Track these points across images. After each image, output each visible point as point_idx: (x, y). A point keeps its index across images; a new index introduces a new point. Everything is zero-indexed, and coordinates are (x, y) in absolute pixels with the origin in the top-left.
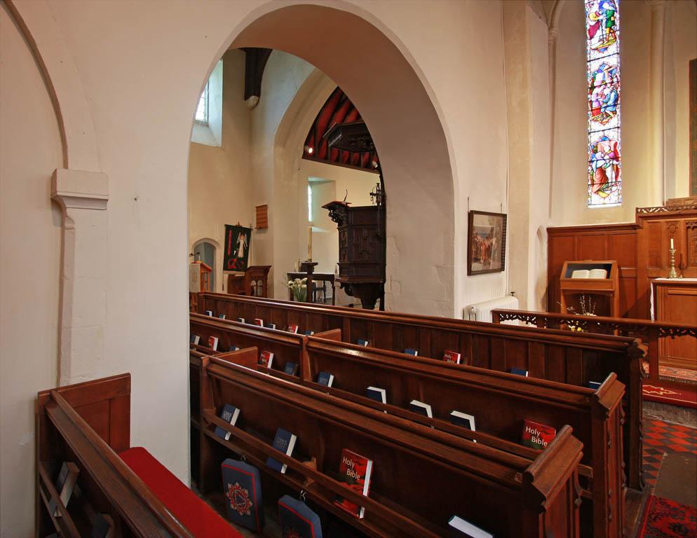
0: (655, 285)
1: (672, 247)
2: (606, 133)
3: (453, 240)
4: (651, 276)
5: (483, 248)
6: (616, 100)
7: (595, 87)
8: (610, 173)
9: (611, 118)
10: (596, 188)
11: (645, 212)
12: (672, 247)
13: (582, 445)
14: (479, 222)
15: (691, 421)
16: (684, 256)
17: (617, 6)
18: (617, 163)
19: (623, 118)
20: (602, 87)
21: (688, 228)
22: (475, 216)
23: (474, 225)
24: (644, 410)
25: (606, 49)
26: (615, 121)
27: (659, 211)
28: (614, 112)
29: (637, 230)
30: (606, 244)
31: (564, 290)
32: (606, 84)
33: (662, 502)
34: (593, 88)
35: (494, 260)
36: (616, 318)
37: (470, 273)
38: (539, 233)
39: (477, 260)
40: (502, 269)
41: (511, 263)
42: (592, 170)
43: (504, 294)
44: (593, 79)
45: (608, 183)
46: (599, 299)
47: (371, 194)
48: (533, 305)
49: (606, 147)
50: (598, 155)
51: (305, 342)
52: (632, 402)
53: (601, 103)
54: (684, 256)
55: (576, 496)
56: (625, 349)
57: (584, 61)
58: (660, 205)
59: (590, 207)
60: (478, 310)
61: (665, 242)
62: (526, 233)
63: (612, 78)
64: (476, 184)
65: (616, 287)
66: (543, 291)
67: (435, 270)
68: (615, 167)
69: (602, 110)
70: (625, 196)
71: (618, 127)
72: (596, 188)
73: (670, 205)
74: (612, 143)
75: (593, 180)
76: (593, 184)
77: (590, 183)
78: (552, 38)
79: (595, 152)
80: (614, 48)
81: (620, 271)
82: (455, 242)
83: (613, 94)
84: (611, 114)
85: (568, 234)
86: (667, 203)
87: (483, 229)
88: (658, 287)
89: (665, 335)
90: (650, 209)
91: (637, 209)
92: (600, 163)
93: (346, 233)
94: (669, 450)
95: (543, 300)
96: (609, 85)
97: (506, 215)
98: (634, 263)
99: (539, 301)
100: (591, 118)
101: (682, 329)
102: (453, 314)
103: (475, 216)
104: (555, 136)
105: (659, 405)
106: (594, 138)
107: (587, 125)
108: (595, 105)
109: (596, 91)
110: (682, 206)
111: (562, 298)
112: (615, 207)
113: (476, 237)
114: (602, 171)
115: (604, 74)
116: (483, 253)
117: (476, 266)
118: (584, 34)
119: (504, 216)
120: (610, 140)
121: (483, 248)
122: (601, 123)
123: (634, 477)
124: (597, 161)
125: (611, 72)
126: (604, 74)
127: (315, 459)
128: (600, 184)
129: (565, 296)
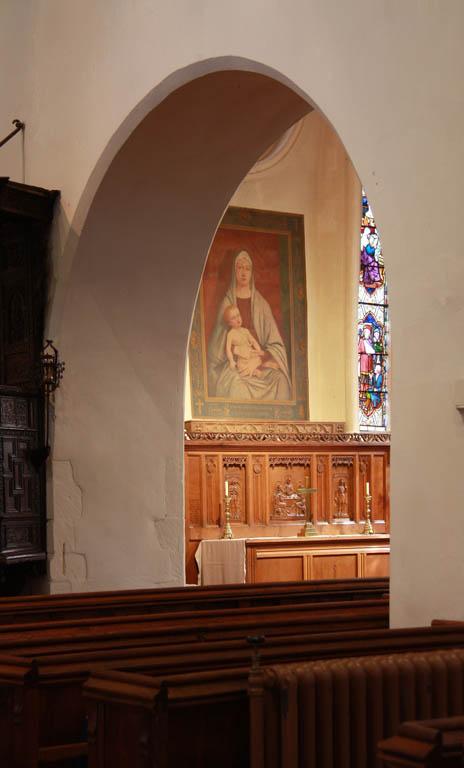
67: (151, 524)
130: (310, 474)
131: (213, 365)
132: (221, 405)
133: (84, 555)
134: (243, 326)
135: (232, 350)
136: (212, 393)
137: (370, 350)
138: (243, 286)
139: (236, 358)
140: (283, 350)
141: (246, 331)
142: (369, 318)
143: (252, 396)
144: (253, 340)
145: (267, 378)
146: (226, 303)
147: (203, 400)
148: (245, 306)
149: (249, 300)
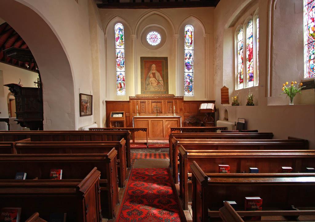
0: (134, 118)
2: (122, 73)
3: (74, 103)
5: (85, 107)
6: (124, 63)
8: (122, 85)
10: (119, 89)
13: (117, 151)
14: (84, 97)
17: (123, 34)
19: (125, 69)
22: (82, 95)
23: (82, 98)
24: (131, 151)
25: (121, 46)
26: (123, 69)
28: (123, 67)
33: (135, 169)
34: (117, 57)
35: (88, 111)
36: (125, 128)
37: (81, 116)
38: (103, 102)
39: (83, 111)
40: (92, 115)
41: (94, 111)
43: (95, 121)
44: (118, 54)
46: (120, 123)
47: (34, 82)
48: (102, 126)
49: (121, 76)
50: (119, 79)
51: (14, 145)
52: (127, 144)
55: (116, 162)
56: (126, 133)
57: (115, 49)
59: (118, 95)
62: (99, 102)
64: (82, 84)
66: (105, 122)
67: (67, 115)
69: (120, 65)
70: (126, 92)
75: (118, 87)
76: (118, 88)
78: (105, 38)
79: (119, 78)
80: (123, 47)
81: (126, 115)
82: (75, 104)
83: (123, 61)
87: (85, 100)
89: (136, 131)
92: (120, 82)
93: (21, 99)
94: (136, 159)
95: (105, 124)
96: (122, 58)
98: (129, 113)
99: (104, 125)
101: (139, 129)
102: (75, 129)
103: (82, 95)
104: (107, 73)
105: (135, 149)
106: (118, 73)
107: (116, 69)
108: (118, 63)
109: (118, 58)
111: (111, 123)
113: (235, 99)
114: (121, 84)
116: (85, 109)
117: (83, 114)
118: (114, 39)
119: (92, 96)
121: (85, 107)
123: (128, 165)
125: (122, 54)
127: (37, 178)
129: (111, 123)
130: (162, 104)
131: (146, 85)
132: (148, 92)
133: (51, 120)
134: (153, 77)
135: (151, 82)
136: (146, 89)
137: (189, 81)
138: (153, 70)
139: (151, 83)
140: (163, 82)
141: (154, 78)
142: (188, 75)
143: (155, 90)
144: (156, 80)
145: (158, 87)
146: (150, 74)
147: (144, 91)
148: (154, 75)
149: (155, 73)
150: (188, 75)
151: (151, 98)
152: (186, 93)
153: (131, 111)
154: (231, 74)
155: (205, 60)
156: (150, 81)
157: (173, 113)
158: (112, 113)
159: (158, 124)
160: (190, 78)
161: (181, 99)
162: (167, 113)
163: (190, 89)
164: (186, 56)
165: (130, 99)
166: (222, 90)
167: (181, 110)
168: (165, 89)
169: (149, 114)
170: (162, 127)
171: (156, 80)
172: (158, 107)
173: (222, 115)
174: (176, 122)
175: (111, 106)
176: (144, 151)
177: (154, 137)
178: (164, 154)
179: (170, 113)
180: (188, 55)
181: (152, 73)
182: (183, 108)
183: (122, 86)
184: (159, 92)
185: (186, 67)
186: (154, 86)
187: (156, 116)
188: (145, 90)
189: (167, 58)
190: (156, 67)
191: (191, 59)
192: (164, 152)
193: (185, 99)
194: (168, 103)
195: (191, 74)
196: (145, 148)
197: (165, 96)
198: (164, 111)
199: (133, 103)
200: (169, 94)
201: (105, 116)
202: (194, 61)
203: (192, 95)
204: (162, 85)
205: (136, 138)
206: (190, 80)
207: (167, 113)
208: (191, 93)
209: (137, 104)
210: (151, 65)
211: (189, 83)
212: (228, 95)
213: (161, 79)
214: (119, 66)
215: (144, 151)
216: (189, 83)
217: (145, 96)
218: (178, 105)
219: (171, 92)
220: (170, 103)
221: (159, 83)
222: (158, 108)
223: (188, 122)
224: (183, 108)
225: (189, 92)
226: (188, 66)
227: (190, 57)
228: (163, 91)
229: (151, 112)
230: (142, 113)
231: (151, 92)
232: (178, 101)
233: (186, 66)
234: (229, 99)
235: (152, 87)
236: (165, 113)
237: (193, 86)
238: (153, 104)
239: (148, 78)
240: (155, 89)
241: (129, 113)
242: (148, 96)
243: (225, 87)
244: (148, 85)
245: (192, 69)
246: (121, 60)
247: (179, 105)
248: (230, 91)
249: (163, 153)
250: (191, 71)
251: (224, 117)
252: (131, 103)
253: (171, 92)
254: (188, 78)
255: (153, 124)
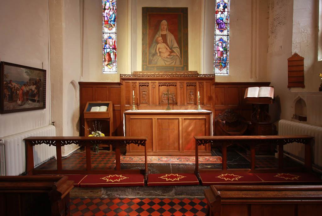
0: (125, 114)
1: (134, 95)
2: (111, 35)
4: (126, 109)
6: (115, 19)
7: (106, 9)
9: (113, 27)
10: (106, 63)
11: (124, 76)
12: (134, 95)
15: (132, 193)
16: (139, 99)
18: (115, 51)
19: (117, 29)
20: (109, 10)
21: (160, 86)
26: (114, 30)
27: (129, 77)
29: (121, 86)
30: (108, 92)
31: (86, 118)
32: (111, 9)
34: (105, 9)
40: (44, 107)
42: (105, 53)
44: (105, 5)
45: (112, 61)
49: (111, 42)
50: (107, 46)
53: (109, 19)
54: (139, 99)
58: (130, 74)
59: (104, 73)
60: (6, 142)
61: (131, 92)
63: (113, 7)
65: (111, 115)
66: (77, 119)
68: (115, 53)
69: (109, 22)
71: (116, 33)
72: (106, 63)
73: (134, 74)
74: (113, 41)
75: (105, 59)
77: (104, 60)
79: (106, 44)
83: (114, 15)
84: (113, 25)
85: (98, 86)
86: (133, 73)
88: (126, 115)
90: (125, 75)
91: (121, 75)
92: (108, 50)
96: (112, 10)
97: (46, 71)
99: (75, 125)
100: (104, 25)
105: (117, 188)
106: (106, 36)
107: (102, 29)
108: (106, 19)
109: (106, 11)
110: (138, 75)
111: (86, 123)
112: (115, 74)
114: (109, 54)
115: (110, 4)
120: (112, 39)
122: (109, 29)
124: (107, 48)
126: (110, 4)
128: (108, 61)
129: (88, 122)
135: (159, 50)
136: (150, 62)
137: (221, 49)
139: (160, 52)
140: (179, 50)
142: (221, 40)
144: (167, 47)
146: (157, 36)
148: (164, 37)
149: (166, 34)
150: (220, 40)
151: (158, 78)
152: (217, 71)
153: (124, 100)
154: (309, 31)
155: (252, 12)
156: (157, 49)
157: (196, 104)
158: (90, 104)
159: (169, 126)
160: (224, 45)
161: (210, 79)
162: (186, 104)
163: (222, 64)
164: (218, 8)
165: (122, 79)
166: (290, 61)
167: (210, 98)
168: (182, 62)
169: (155, 106)
170: (176, 132)
171: (169, 47)
172: (170, 94)
173: (289, 108)
174: (203, 122)
175: (89, 92)
176: (138, 193)
177: (163, 150)
178: (182, 204)
179: (191, 104)
180: (222, 6)
181: (161, 35)
182: (214, 96)
183: (111, 59)
184: (172, 68)
185: (217, 27)
186: (164, 58)
187: (167, 109)
188: (149, 64)
189: (186, 9)
190: (168, 25)
191: (226, 13)
192: (181, 195)
193: (217, 80)
194: (188, 87)
195: (225, 39)
196: (141, 186)
197: (182, 73)
198: (181, 102)
199: (127, 86)
200: (190, 70)
201: (78, 109)
202: (230, 16)
203: (227, 74)
204: (177, 55)
205: (129, 152)
206: (223, 47)
207: (186, 104)
208: (224, 71)
209: (134, 88)
210: (160, 22)
211: (222, 54)
212: (303, 71)
213: (176, 45)
214: (108, 23)
215: (138, 193)
216: (222, 54)
217: (149, 74)
218: (205, 90)
219: (192, 68)
220: (191, 87)
221: (172, 52)
222: (170, 96)
223: (224, 122)
224: (214, 96)
225: (221, 68)
226: (220, 25)
227: (224, 9)
228: (180, 66)
229: (158, 103)
230: (142, 103)
231: (158, 68)
232: (205, 83)
233: (218, 24)
234: (303, 79)
235: (160, 58)
236: (183, 105)
237: (228, 59)
238: (162, 88)
239: (154, 44)
240: (166, 62)
241: (120, 104)
242: (153, 73)
243: (296, 55)
244: (154, 55)
245: (226, 31)
246: (111, 13)
247: (207, 91)
248: (307, 63)
249: (180, 196)
250: (225, 32)
251: (294, 113)
252: (123, 87)
253: (192, 68)
254: (220, 44)
255: (160, 126)
